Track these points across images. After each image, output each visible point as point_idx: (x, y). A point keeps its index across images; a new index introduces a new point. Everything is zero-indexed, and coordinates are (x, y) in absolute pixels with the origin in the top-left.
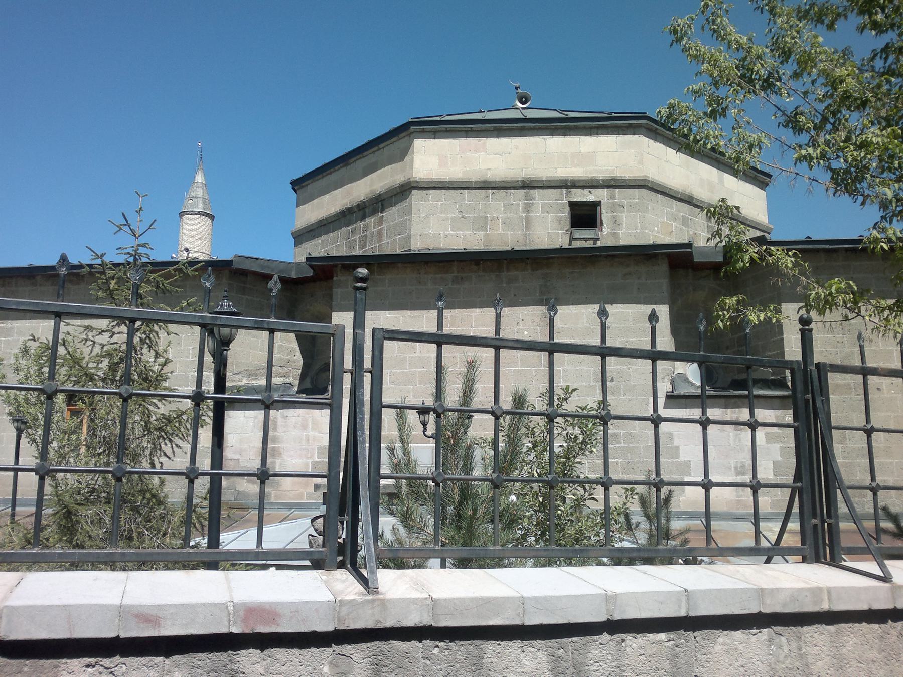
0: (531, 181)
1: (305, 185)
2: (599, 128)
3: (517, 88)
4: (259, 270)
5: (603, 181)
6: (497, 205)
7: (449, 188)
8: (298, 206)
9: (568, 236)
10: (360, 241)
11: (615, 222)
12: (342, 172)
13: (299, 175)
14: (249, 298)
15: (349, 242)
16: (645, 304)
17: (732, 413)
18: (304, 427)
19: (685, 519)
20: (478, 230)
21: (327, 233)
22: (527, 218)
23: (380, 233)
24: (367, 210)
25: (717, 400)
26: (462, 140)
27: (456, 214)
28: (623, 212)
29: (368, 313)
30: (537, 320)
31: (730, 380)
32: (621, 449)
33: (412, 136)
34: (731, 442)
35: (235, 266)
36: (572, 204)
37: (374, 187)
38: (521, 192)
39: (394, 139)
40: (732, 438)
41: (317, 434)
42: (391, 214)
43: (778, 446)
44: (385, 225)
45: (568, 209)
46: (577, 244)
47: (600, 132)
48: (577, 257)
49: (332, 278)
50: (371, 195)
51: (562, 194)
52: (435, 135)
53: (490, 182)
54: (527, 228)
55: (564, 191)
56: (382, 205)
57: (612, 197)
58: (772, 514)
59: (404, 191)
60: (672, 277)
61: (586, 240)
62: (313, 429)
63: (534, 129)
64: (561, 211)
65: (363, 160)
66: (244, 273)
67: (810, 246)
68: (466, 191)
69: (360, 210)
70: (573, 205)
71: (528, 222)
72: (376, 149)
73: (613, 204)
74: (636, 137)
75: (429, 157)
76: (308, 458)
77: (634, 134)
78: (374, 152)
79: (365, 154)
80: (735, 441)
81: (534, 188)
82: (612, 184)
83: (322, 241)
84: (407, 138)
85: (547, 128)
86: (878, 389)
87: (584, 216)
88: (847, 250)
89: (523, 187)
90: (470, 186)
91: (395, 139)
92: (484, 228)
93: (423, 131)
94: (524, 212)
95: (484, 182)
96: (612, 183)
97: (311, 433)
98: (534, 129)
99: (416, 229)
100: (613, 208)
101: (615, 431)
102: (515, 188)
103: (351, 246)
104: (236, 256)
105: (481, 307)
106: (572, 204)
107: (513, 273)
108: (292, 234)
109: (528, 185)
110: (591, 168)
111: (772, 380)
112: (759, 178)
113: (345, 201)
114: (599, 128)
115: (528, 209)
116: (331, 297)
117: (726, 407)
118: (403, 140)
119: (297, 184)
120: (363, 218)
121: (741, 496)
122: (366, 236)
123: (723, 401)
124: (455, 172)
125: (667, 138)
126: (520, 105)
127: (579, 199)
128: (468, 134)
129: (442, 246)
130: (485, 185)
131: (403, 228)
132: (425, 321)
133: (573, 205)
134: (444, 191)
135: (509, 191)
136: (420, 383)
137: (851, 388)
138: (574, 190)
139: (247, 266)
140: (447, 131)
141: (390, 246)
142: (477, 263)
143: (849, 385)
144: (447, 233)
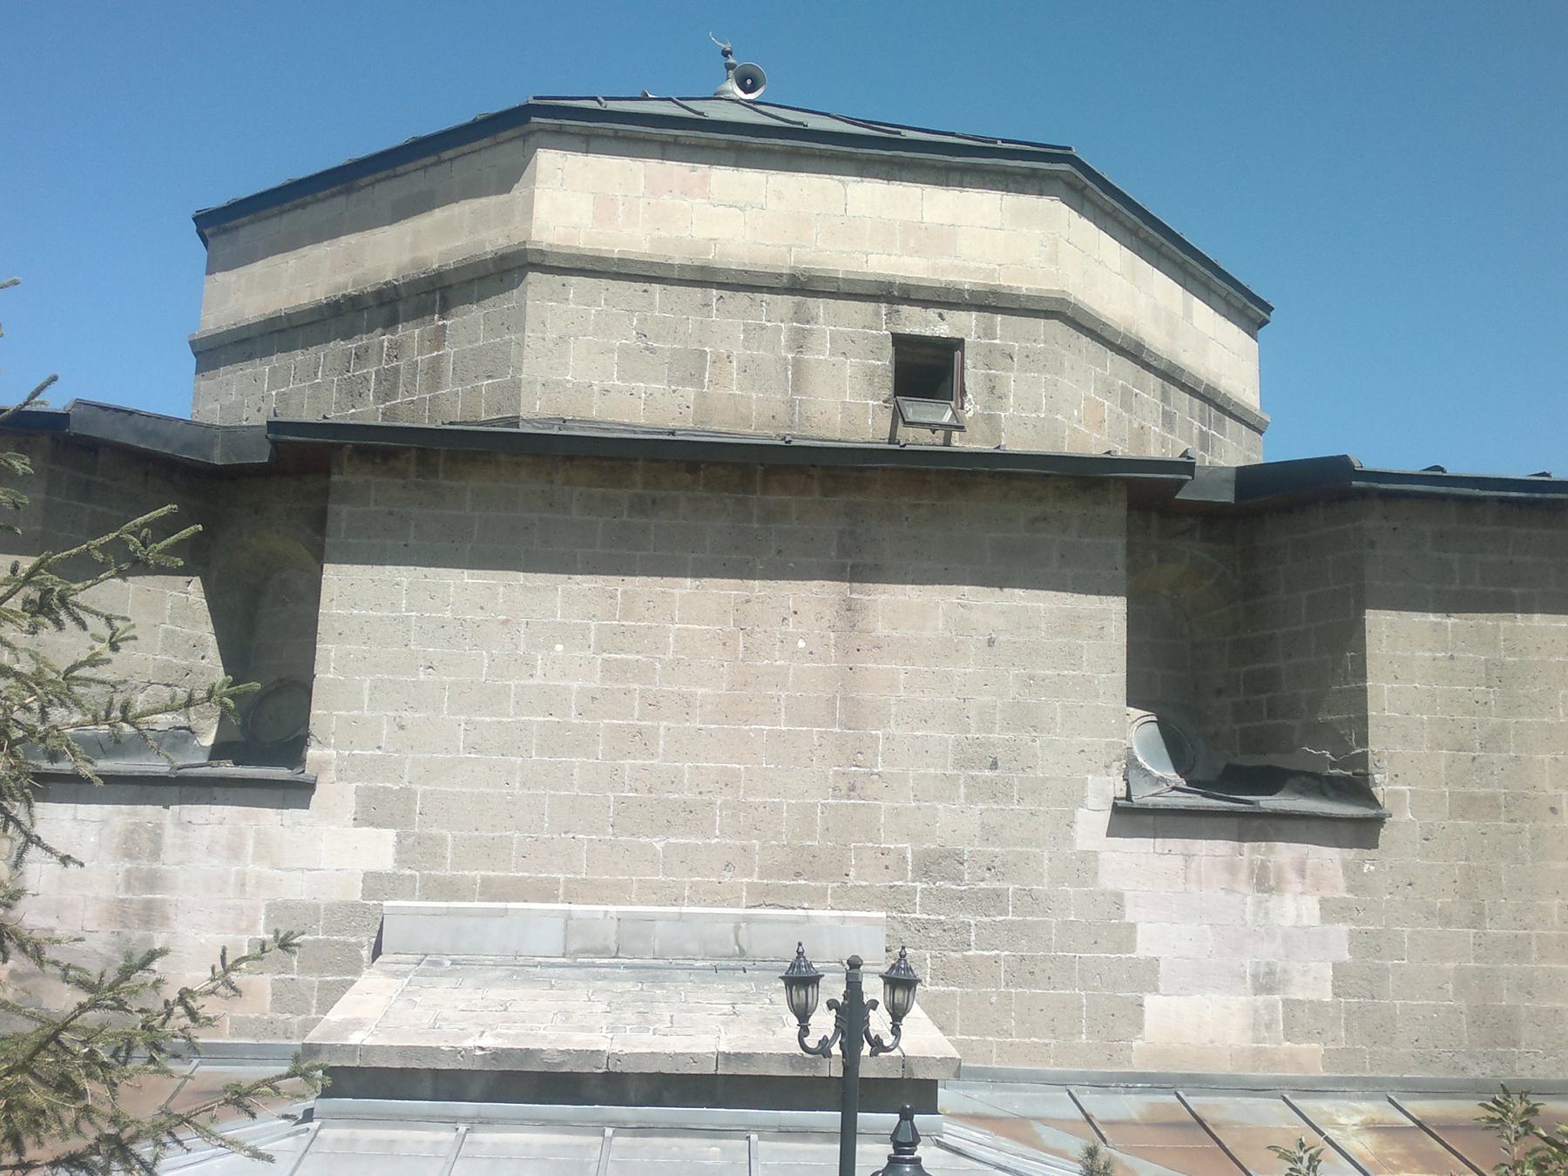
0: (811, 279)
3: (726, 54)
4: (132, 441)
5: (971, 293)
7: (617, 276)
8: (210, 272)
9: (889, 413)
10: (379, 382)
11: (993, 389)
12: (338, 205)
13: (217, 199)
15: (349, 381)
16: (1074, 591)
17: (1253, 851)
18: (235, 852)
19: (1143, 1091)
20: (683, 381)
21: (288, 348)
22: (797, 363)
23: (435, 369)
24: (401, 307)
25: (1222, 821)
26: (652, 163)
27: (632, 340)
28: (1011, 369)
30: (829, 614)
31: (1221, 765)
32: (1009, 927)
33: (532, 140)
34: (1248, 917)
35: (74, 428)
36: (900, 341)
37: (424, 253)
38: (786, 302)
39: (485, 142)
40: (1249, 909)
41: (266, 871)
42: (469, 325)
43: (1344, 928)
44: (449, 350)
45: (889, 351)
46: (913, 438)
47: (967, 179)
48: (927, 472)
49: (328, 473)
50: (413, 273)
51: (877, 314)
52: (589, 143)
53: (715, 271)
54: (797, 388)
56: (443, 298)
57: (989, 332)
58: (1326, 1080)
59: (508, 270)
61: (933, 427)
63: (821, 156)
65: (396, 183)
66: (90, 447)
67: (1442, 490)
68: (657, 287)
69: (381, 305)
70: (902, 343)
71: (799, 374)
72: (432, 159)
73: (991, 349)
74: (1044, 201)
75: (573, 197)
76: (241, 931)
77: (1041, 194)
78: (425, 167)
79: (401, 169)
80: (1255, 915)
82: (990, 302)
83: (273, 371)
84: (519, 143)
85: (849, 158)
86: (1553, 810)
87: (925, 370)
88: (1502, 500)
90: (658, 275)
91: (497, 140)
92: (695, 378)
93: (560, 131)
94: (790, 349)
95: (702, 268)
96: (992, 301)
97: (253, 868)
98: (821, 156)
99: (533, 369)
100: (992, 357)
101: (996, 885)
102: (771, 290)
103: (353, 392)
104: (79, 403)
106: (900, 341)
107: (776, 498)
108: (192, 344)
109: (802, 286)
110: (944, 261)
111: (1330, 778)
112: (1247, 309)
115: (799, 342)
116: (320, 522)
117: (1241, 838)
118: (507, 147)
119: (212, 224)
120: (391, 323)
121: (1264, 1040)
122: (396, 370)
123: (1234, 822)
124: (632, 238)
125: (1101, 209)
126: (740, 94)
127: (916, 331)
128: (666, 150)
130: (704, 278)
132: (559, 600)
133: (902, 343)
134: (604, 282)
135: (758, 296)
137: (1499, 806)
138: (905, 309)
139: (104, 430)
140: (616, 136)
141: (459, 402)
142: (693, 468)
143: (1494, 797)
144: (607, 384)
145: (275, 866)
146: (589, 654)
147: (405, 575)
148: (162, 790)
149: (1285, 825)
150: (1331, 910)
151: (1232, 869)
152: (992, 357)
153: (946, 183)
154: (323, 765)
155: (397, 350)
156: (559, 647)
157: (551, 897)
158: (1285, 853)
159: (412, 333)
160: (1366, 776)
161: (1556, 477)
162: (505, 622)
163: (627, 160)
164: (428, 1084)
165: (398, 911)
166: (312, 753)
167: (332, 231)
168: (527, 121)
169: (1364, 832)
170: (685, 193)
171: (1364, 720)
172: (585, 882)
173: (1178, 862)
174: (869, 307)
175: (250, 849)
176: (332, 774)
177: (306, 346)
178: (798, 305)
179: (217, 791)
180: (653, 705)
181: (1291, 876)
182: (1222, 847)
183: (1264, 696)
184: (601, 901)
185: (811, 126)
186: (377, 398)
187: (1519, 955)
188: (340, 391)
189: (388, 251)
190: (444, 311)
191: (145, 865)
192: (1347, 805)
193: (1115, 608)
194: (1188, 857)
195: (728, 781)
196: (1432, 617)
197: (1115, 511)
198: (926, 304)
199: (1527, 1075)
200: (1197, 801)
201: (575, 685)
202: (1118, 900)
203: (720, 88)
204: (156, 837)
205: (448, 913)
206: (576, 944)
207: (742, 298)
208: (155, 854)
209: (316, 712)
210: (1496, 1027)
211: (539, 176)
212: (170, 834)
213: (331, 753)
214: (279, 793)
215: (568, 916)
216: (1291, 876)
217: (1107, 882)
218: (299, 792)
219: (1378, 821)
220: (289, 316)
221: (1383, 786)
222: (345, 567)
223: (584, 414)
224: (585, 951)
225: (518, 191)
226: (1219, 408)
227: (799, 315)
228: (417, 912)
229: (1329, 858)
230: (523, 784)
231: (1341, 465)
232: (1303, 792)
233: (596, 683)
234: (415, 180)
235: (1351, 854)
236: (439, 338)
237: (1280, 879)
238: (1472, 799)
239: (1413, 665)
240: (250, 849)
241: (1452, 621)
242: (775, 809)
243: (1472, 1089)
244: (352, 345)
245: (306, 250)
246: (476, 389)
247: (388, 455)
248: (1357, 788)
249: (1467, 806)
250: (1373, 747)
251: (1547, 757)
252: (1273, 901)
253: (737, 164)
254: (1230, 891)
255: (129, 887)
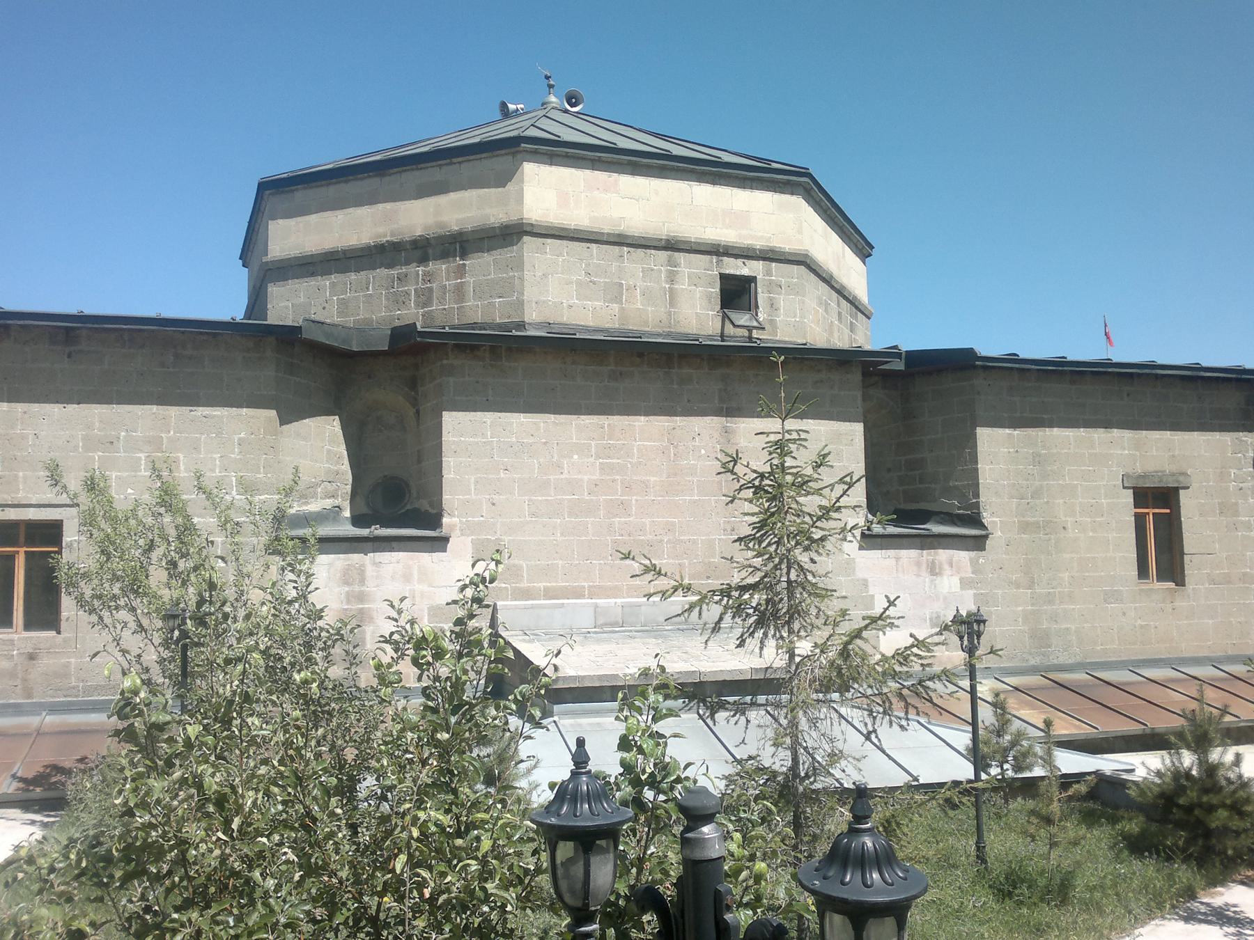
0: (677, 242)
1: (279, 193)
2: (753, 179)
3: (547, 78)
5: (760, 251)
6: (636, 269)
9: (720, 319)
11: (772, 305)
12: (372, 183)
14: (298, 380)
18: (407, 578)
20: (611, 301)
22: (671, 290)
23: (460, 291)
26: (588, 172)
27: (582, 277)
29: (447, 416)
30: (716, 435)
33: (519, 156)
38: (663, 255)
41: (425, 588)
42: (481, 266)
43: (971, 592)
44: (469, 279)
50: (441, 232)
55: (714, 258)
56: (461, 247)
57: (769, 273)
60: (865, 386)
62: (420, 581)
63: (678, 170)
64: (711, 285)
65: (417, 173)
70: (724, 278)
73: (771, 282)
74: (794, 197)
75: (544, 192)
78: (440, 166)
81: (679, 250)
82: (769, 256)
83: (333, 285)
85: (692, 171)
89: (665, 248)
90: (596, 239)
91: (499, 155)
92: (617, 299)
93: (535, 152)
94: (667, 282)
95: (619, 235)
96: (771, 255)
97: (419, 587)
99: (530, 293)
100: (774, 287)
102: (656, 248)
105: (646, 414)
107: (686, 371)
109: (672, 246)
110: (744, 232)
111: (958, 515)
112: (863, 249)
113: (381, 230)
114: (753, 179)
120: (423, 260)
123: (918, 540)
124: (578, 217)
128: (595, 164)
129: (565, 320)
130: (620, 241)
131: (511, 287)
133: (724, 278)
134: (565, 242)
136: (570, 515)
138: (725, 259)
140: (567, 156)
142: (641, 355)
143: (1038, 523)
145: (431, 585)
146: (592, 460)
147: (488, 417)
148: (364, 545)
149: (942, 540)
150: (965, 583)
151: (918, 564)
152: (774, 287)
153: (744, 187)
154: (452, 527)
155: (429, 277)
156: (576, 457)
157: (581, 596)
158: (943, 555)
159: (441, 268)
160: (979, 514)
161: (1069, 359)
162: (545, 443)
163: (573, 170)
164: (608, 694)
165: (506, 608)
166: (445, 520)
167: (372, 200)
168: (519, 145)
169: (978, 543)
170: (606, 190)
171: (978, 484)
172: (600, 587)
173: (893, 561)
174: (708, 257)
175: (416, 577)
176: (458, 532)
177: (357, 271)
178: (670, 257)
179: (394, 544)
180: (628, 487)
181: (946, 567)
182: (913, 553)
183: (917, 472)
184: (608, 597)
185: (674, 153)
186: (417, 305)
187: (1050, 602)
188: (388, 299)
189: (416, 216)
190: (464, 255)
191: (357, 588)
192: (967, 526)
193: (858, 428)
194: (898, 559)
195: (670, 528)
196: (1007, 431)
197: (856, 377)
198: (736, 256)
199: (1055, 662)
200: (892, 530)
201: (586, 478)
202: (865, 583)
203: (546, 100)
204: (362, 572)
205: (533, 607)
206: (600, 622)
207: (640, 252)
208: (362, 581)
209: (446, 497)
210: (1041, 639)
211: (526, 179)
212: (370, 571)
213: (455, 520)
214: (429, 544)
215: (596, 606)
216: (946, 567)
217: (860, 574)
218: (440, 543)
219: (986, 537)
220: (344, 252)
221: (987, 518)
222: (454, 413)
223: (559, 320)
224: (606, 624)
225: (510, 186)
226: (857, 308)
227: (672, 263)
228: (516, 607)
229: (963, 557)
230: (562, 534)
231: (969, 353)
232: (942, 523)
233: (596, 477)
234: (434, 173)
235: (973, 554)
236: (461, 272)
237: (940, 568)
238: (1028, 524)
239: (999, 453)
240: (416, 577)
241: (1017, 432)
242: (695, 542)
243: (1034, 670)
244: (394, 272)
245: (351, 210)
246: (492, 304)
247: (473, 348)
248: (974, 520)
249: (1025, 527)
250: (982, 499)
251: (1061, 501)
252: (938, 580)
253: (633, 174)
254: (918, 576)
255: (348, 602)
